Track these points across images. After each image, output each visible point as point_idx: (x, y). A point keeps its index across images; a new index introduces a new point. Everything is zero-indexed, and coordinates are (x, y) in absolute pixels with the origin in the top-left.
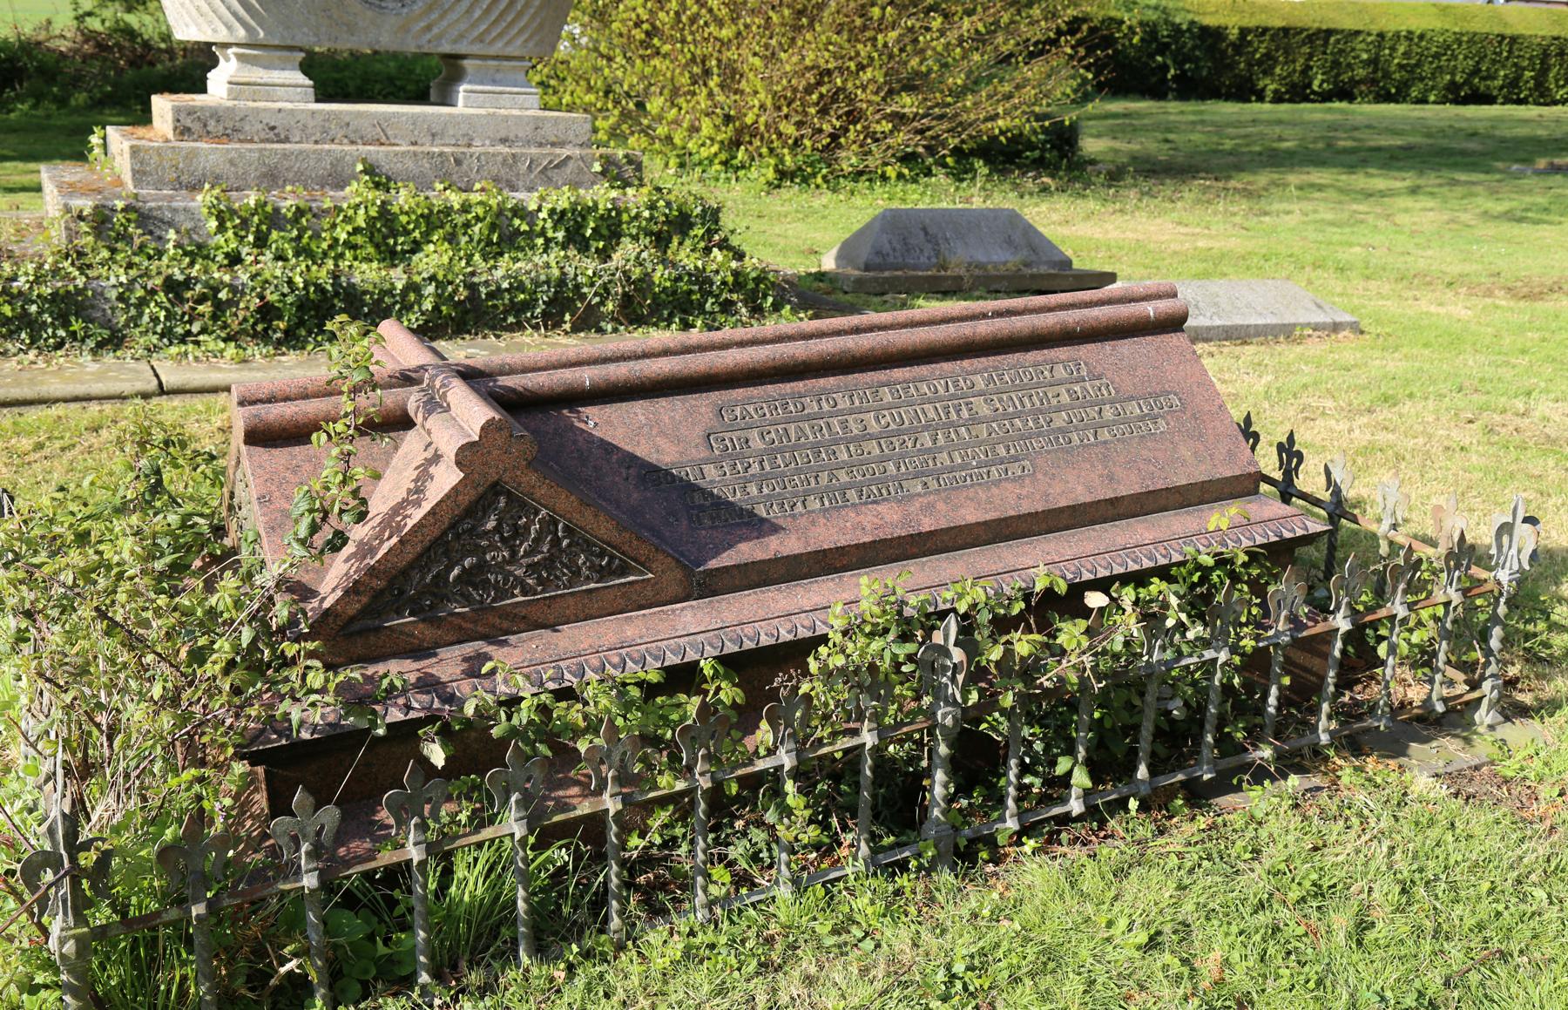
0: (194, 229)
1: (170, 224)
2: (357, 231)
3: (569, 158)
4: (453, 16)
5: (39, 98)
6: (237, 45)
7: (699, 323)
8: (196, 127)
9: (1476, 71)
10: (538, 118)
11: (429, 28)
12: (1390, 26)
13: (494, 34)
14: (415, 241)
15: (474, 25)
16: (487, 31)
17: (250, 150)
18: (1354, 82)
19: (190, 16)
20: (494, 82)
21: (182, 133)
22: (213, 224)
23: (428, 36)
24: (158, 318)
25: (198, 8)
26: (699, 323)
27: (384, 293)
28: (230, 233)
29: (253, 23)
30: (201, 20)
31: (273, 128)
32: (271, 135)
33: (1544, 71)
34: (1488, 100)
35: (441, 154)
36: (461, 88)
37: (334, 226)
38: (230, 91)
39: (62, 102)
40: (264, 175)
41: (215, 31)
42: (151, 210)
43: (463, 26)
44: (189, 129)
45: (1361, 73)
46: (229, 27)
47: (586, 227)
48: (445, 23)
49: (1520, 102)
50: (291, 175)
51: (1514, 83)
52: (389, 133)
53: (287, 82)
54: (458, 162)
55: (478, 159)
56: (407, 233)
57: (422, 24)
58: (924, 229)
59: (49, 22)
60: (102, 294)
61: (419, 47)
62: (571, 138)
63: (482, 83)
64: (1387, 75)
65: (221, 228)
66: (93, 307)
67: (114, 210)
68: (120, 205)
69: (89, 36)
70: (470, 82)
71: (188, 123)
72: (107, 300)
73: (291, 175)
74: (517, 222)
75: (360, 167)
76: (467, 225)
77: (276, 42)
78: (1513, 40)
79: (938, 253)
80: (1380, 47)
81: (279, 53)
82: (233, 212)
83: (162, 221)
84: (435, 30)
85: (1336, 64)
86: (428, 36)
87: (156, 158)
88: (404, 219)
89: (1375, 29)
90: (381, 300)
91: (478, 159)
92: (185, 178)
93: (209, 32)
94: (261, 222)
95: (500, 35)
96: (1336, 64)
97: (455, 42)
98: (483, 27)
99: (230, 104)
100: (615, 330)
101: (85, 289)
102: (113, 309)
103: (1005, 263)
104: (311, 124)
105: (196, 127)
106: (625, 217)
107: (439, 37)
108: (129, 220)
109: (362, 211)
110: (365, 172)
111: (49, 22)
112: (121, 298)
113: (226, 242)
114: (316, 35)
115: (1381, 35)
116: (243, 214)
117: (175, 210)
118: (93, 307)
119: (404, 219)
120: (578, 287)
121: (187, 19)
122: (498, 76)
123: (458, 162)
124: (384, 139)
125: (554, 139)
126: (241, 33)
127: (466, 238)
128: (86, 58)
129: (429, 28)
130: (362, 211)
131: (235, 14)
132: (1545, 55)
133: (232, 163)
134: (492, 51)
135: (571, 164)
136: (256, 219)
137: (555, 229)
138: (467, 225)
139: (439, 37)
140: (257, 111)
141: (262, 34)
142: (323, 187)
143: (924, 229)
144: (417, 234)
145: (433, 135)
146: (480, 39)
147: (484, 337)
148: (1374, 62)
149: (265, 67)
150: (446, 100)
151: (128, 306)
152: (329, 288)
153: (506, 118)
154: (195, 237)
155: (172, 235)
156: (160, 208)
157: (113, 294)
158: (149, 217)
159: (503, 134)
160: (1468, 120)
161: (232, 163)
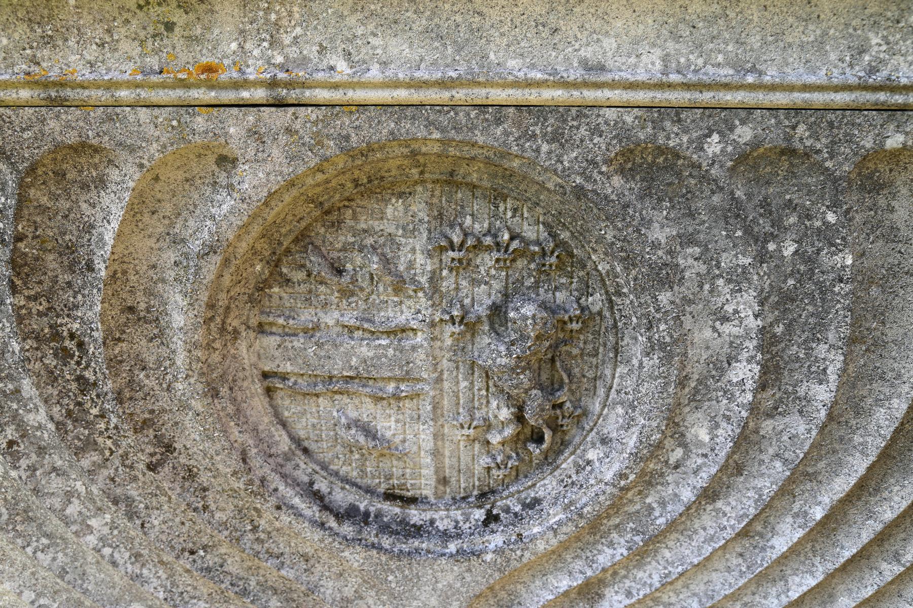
4: (686, 551)
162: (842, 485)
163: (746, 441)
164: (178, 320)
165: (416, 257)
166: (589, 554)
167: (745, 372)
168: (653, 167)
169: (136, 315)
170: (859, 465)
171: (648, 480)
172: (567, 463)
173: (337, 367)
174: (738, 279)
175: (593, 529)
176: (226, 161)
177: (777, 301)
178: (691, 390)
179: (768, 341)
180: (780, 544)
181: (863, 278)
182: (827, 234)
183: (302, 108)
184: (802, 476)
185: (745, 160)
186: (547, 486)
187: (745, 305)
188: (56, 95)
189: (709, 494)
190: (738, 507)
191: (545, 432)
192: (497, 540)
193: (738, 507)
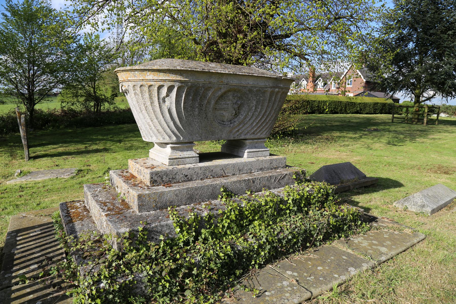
0: (170, 233)
1: (160, 233)
2: (232, 221)
3: (286, 175)
4: (247, 126)
5: (53, 126)
6: (172, 143)
7: (343, 236)
8: (159, 180)
9: (335, 108)
10: (271, 160)
11: (238, 131)
12: (321, 100)
13: (258, 131)
14: (250, 220)
15: (253, 128)
16: (256, 130)
17: (183, 189)
18: (315, 110)
19: (153, 132)
20: (256, 148)
21: (153, 183)
22: (178, 230)
23: (238, 133)
24: (166, 287)
25: (158, 130)
26: (343, 236)
27: (251, 251)
28: (185, 233)
29: (179, 135)
30: (158, 135)
31: (187, 176)
32: (186, 178)
33: (346, 108)
34: (337, 113)
35: (249, 180)
36: (246, 151)
37: (222, 220)
38: (169, 162)
39: (58, 127)
40: (188, 198)
41: (164, 139)
42: (153, 228)
43: (249, 129)
44: (156, 181)
45: (316, 108)
46: (170, 137)
47: (302, 203)
48: (244, 128)
49: (343, 113)
50: (197, 197)
51: (341, 110)
52: (226, 172)
53: (190, 156)
54: (254, 182)
55: (260, 180)
56: (247, 217)
57: (237, 129)
58: (334, 171)
59: (55, 109)
60: (141, 281)
61: (234, 138)
62: (280, 165)
63: (252, 148)
64: (321, 109)
65: (182, 231)
66: (137, 288)
67: (137, 231)
68: (140, 229)
69: (63, 111)
70: (248, 148)
71: (156, 178)
72: (143, 283)
73: (197, 197)
74: (281, 206)
75: (222, 190)
76: (266, 210)
77: (187, 141)
78: (341, 102)
79: (340, 179)
80: (319, 103)
81: (186, 145)
82: (186, 223)
83: (157, 232)
84: (240, 131)
85: (312, 107)
86: (238, 133)
87: (148, 199)
88: (246, 213)
89: (318, 100)
90: (249, 254)
91: (260, 180)
92: (159, 205)
93: (161, 139)
94: (196, 225)
95: (260, 131)
96: (312, 107)
97: (245, 135)
98: (255, 129)
99: (170, 168)
100: (320, 245)
101: (133, 280)
102: (146, 287)
103: (354, 179)
104: (200, 172)
105: (159, 180)
106: (312, 197)
107: (241, 133)
108: (144, 235)
109: (233, 213)
110: (224, 191)
111: (55, 109)
112: (149, 281)
113: (184, 237)
114: (201, 137)
115: (319, 101)
116: (190, 222)
117: (162, 226)
118: (137, 288)
119: (246, 213)
120: (310, 231)
121: (152, 134)
122: (256, 145)
123: (254, 182)
124: (224, 175)
125: (275, 166)
126: (174, 139)
127: (266, 216)
128: (63, 116)
129: (238, 131)
130: (233, 213)
131: (173, 132)
132: (346, 105)
133: (176, 195)
134: (256, 137)
135: (287, 177)
136: (194, 224)
137: (294, 206)
138: (266, 210)
139: (241, 133)
140: (181, 170)
141: (182, 138)
142: (209, 199)
143: (334, 171)
144: (251, 218)
145: (240, 171)
146: (253, 133)
147: (283, 260)
148: (318, 106)
149: (181, 151)
150: (242, 157)
151: (152, 283)
152: (232, 255)
153: (262, 161)
154: (170, 236)
155: (162, 238)
156: (156, 226)
157: (146, 280)
158: (152, 231)
159: (261, 167)
160: (340, 118)
161: (176, 195)
162: (259, 119)
163: (253, 115)
164: (213, 103)
165: (231, 97)
166: (293, 92)
167: (254, 108)
168: (250, 91)
169: (209, 103)
170: (261, 117)
171: (245, 119)
172: (238, 117)
173: (222, 108)
174: (254, 100)
175: (240, 124)
176: (220, 89)
177: (257, 102)
178: (250, 110)
179: (256, 105)
180: (254, 125)
181: (263, 100)
182: (261, 97)
183: (165, 68)
184: (257, 118)
185: (257, 90)
186: (236, 120)
187: (255, 102)
188: (210, 83)
189: (249, 120)
190: (252, 121)
191: (236, 115)
192: (232, 125)
193: (252, 121)
